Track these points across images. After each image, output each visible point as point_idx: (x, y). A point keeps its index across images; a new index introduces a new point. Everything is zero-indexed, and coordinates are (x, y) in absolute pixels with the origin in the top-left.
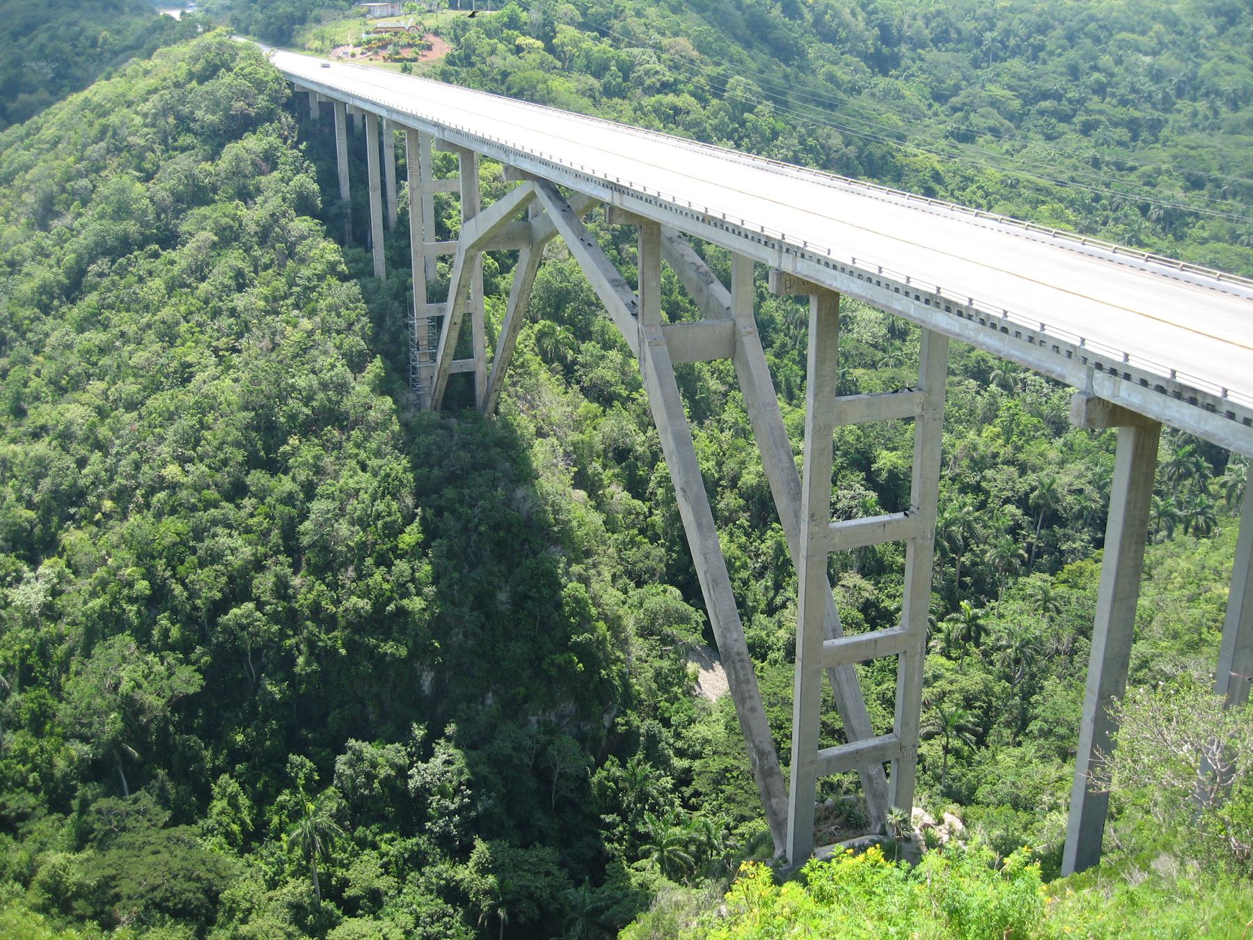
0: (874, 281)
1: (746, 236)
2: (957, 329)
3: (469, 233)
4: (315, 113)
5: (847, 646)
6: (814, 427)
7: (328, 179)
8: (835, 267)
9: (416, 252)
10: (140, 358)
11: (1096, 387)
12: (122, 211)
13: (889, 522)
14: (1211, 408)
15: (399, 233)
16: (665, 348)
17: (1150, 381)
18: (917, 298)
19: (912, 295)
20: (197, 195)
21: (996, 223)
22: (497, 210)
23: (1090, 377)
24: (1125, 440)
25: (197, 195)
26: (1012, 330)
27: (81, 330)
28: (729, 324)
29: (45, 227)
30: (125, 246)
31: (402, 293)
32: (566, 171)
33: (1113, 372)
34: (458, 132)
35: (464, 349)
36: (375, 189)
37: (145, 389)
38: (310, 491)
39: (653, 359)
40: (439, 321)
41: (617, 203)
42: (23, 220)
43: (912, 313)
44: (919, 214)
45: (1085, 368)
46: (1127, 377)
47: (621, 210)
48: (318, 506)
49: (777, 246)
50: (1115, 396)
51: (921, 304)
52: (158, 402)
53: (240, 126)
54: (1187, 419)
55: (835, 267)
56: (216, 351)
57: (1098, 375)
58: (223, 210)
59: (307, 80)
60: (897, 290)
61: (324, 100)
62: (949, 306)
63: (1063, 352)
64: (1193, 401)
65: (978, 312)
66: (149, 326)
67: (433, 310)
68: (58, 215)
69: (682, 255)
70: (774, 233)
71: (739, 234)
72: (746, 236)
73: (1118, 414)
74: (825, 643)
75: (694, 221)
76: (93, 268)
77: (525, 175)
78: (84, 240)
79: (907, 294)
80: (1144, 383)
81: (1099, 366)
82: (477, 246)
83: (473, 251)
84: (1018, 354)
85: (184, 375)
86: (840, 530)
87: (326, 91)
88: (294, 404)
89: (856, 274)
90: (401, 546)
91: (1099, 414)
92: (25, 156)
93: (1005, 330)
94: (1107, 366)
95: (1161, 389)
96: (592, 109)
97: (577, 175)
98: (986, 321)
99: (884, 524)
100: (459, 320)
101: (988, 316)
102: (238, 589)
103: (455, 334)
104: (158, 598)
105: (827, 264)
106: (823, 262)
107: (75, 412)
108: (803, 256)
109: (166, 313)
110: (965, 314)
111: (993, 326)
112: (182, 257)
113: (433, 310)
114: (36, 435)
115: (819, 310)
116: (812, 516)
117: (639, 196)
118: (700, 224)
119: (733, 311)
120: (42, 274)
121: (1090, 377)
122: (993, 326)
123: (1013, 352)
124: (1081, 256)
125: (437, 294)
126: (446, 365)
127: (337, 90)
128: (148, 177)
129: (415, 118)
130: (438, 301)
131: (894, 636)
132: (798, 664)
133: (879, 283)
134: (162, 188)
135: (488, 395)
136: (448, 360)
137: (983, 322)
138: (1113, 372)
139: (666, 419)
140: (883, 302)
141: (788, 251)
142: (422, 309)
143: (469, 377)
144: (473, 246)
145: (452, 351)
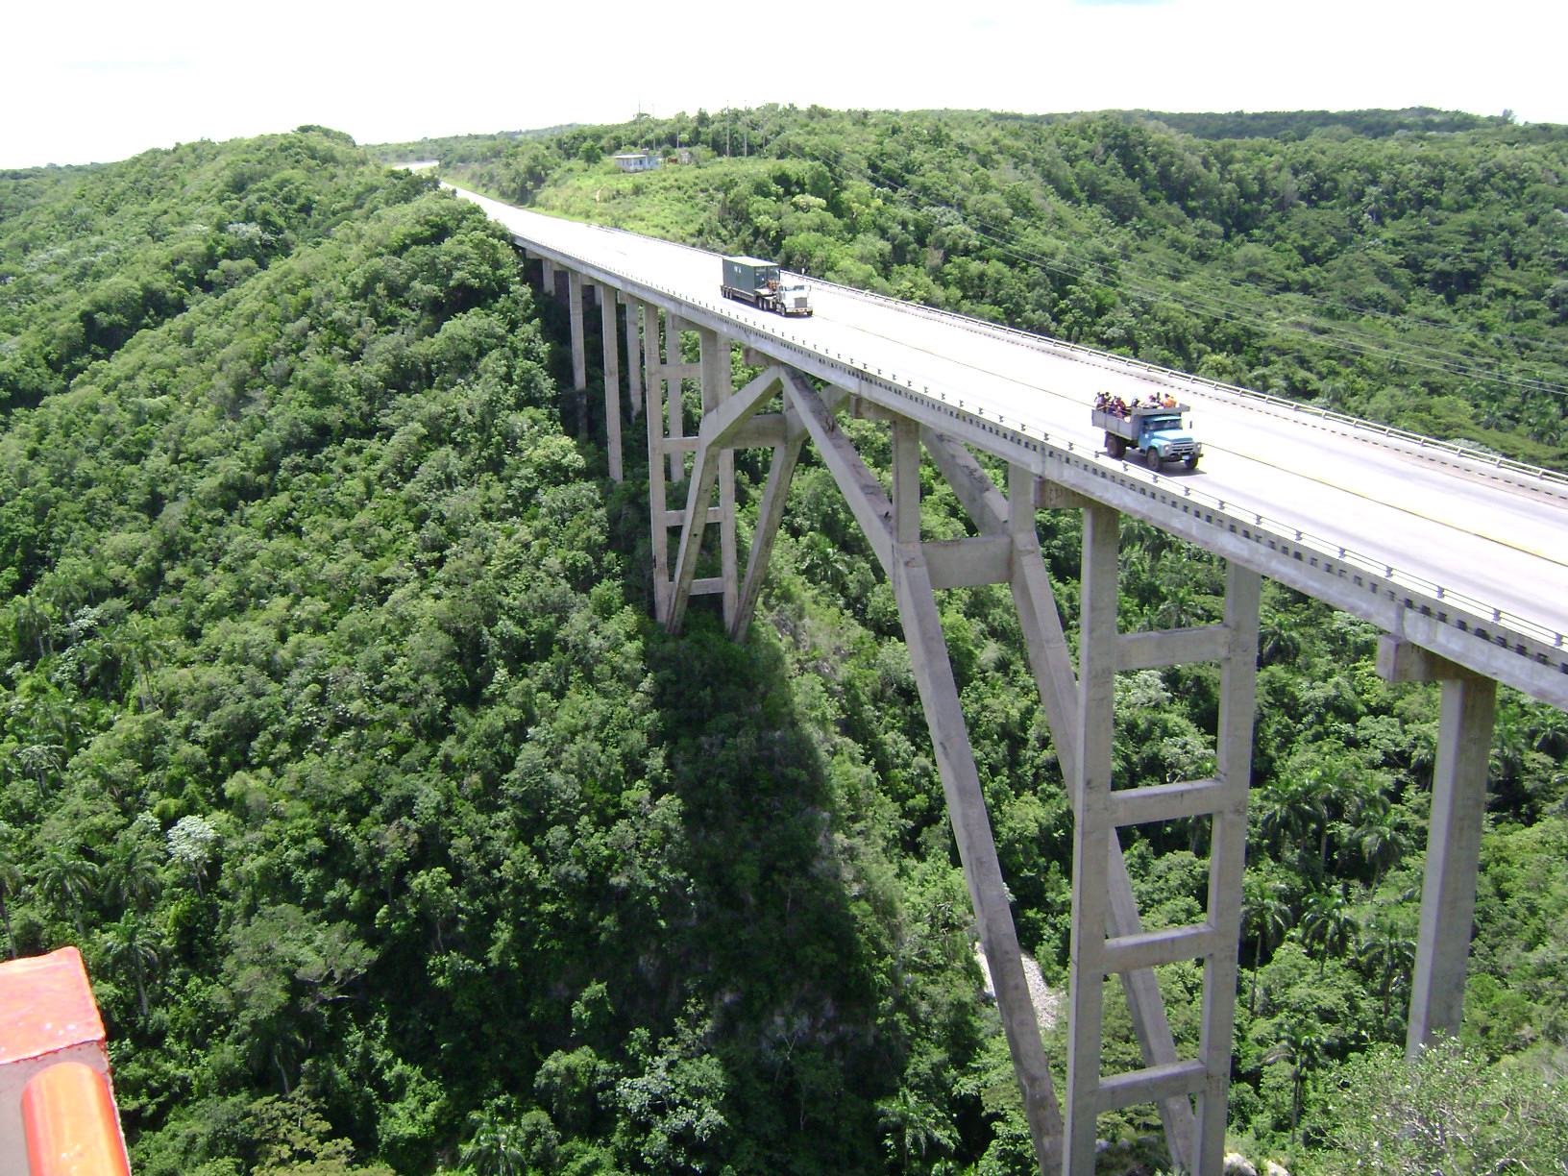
0: (1148, 492)
1: (1005, 436)
2: (1245, 554)
3: (712, 426)
4: (549, 284)
5: (1138, 946)
6: (1090, 672)
7: (560, 367)
8: (1104, 475)
9: (654, 449)
10: (333, 569)
11: (1408, 630)
12: (324, 395)
13: (1189, 791)
14: (1543, 659)
15: (635, 424)
16: (925, 569)
17: (1470, 624)
18: (1198, 514)
19: (1191, 510)
20: (407, 377)
21: (1321, 419)
22: (736, 405)
23: (1401, 617)
24: (1446, 696)
25: (407, 377)
26: (1306, 557)
27: (268, 534)
28: (1006, 540)
29: (237, 417)
30: (324, 434)
31: (638, 502)
32: (809, 354)
33: (1426, 611)
34: (694, 308)
35: (709, 565)
36: (611, 373)
37: (334, 607)
38: (518, 733)
39: (910, 585)
40: (675, 532)
41: (865, 395)
42: (212, 407)
43: (1194, 532)
44: (1228, 407)
45: (1393, 605)
46: (1443, 618)
47: (870, 403)
48: (530, 754)
49: (1038, 449)
50: (1430, 641)
51: (1201, 521)
52: (354, 619)
53: (466, 298)
54: (1517, 672)
55: (1104, 475)
56: (419, 566)
57: (1409, 614)
58: (429, 403)
59: (539, 246)
60: (1174, 504)
61: (557, 268)
62: (1233, 526)
63: (1367, 586)
64: (1521, 650)
65: (1267, 533)
66: (344, 534)
67: (672, 517)
68: (250, 400)
69: (953, 456)
70: (1035, 433)
71: (997, 433)
72: (1005, 436)
73: (1437, 667)
74: (1111, 942)
75: (948, 416)
76: (286, 462)
77: (769, 361)
78: (274, 435)
79: (1186, 509)
80: (1462, 626)
81: (1409, 604)
82: (721, 442)
83: (715, 449)
84: (1316, 585)
85: (381, 590)
86: (1125, 801)
87: (559, 258)
88: (506, 625)
89: (1127, 484)
90: (624, 802)
91: (1416, 668)
92: (221, 334)
93: (1298, 556)
94: (1417, 603)
95: (1482, 634)
96: (878, 281)
97: (822, 360)
98: (1275, 544)
99: (1182, 794)
100: (700, 531)
101: (1279, 538)
102: (430, 849)
103: (695, 548)
104: (333, 857)
105: (1095, 471)
106: (1090, 468)
107: (254, 630)
108: (1068, 461)
109: (362, 518)
110: (1252, 535)
111: (1285, 550)
112: (387, 451)
113: (672, 517)
114: (210, 659)
115: (1094, 527)
116: (1088, 783)
117: (888, 387)
118: (953, 419)
119: (1010, 525)
120: (230, 467)
121: (1401, 617)
122: (1285, 550)
123: (1311, 583)
124: (1420, 462)
125: (676, 499)
126: (685, 585)
127: (569, 257)
128: (355, 356)
129: (649, 290)
130: (677, 509)
131: (1198, 935)
132: (1072, 968)
133: (1153, 496)
134: (373, 369)
135: (739, 619)
136: (687, 579)
137: (1272, 545)
138: (1426, 611)
139: (1410, 639)
140: (1161, 518)
141: (1051, 454)
142: (661, 517)
143: (715, 601)
144: (714, 444)
145: (691, 568)
